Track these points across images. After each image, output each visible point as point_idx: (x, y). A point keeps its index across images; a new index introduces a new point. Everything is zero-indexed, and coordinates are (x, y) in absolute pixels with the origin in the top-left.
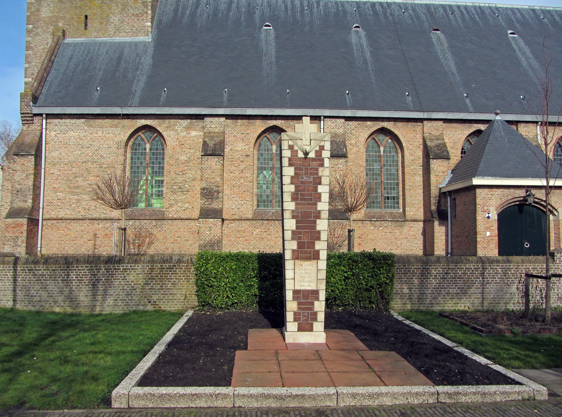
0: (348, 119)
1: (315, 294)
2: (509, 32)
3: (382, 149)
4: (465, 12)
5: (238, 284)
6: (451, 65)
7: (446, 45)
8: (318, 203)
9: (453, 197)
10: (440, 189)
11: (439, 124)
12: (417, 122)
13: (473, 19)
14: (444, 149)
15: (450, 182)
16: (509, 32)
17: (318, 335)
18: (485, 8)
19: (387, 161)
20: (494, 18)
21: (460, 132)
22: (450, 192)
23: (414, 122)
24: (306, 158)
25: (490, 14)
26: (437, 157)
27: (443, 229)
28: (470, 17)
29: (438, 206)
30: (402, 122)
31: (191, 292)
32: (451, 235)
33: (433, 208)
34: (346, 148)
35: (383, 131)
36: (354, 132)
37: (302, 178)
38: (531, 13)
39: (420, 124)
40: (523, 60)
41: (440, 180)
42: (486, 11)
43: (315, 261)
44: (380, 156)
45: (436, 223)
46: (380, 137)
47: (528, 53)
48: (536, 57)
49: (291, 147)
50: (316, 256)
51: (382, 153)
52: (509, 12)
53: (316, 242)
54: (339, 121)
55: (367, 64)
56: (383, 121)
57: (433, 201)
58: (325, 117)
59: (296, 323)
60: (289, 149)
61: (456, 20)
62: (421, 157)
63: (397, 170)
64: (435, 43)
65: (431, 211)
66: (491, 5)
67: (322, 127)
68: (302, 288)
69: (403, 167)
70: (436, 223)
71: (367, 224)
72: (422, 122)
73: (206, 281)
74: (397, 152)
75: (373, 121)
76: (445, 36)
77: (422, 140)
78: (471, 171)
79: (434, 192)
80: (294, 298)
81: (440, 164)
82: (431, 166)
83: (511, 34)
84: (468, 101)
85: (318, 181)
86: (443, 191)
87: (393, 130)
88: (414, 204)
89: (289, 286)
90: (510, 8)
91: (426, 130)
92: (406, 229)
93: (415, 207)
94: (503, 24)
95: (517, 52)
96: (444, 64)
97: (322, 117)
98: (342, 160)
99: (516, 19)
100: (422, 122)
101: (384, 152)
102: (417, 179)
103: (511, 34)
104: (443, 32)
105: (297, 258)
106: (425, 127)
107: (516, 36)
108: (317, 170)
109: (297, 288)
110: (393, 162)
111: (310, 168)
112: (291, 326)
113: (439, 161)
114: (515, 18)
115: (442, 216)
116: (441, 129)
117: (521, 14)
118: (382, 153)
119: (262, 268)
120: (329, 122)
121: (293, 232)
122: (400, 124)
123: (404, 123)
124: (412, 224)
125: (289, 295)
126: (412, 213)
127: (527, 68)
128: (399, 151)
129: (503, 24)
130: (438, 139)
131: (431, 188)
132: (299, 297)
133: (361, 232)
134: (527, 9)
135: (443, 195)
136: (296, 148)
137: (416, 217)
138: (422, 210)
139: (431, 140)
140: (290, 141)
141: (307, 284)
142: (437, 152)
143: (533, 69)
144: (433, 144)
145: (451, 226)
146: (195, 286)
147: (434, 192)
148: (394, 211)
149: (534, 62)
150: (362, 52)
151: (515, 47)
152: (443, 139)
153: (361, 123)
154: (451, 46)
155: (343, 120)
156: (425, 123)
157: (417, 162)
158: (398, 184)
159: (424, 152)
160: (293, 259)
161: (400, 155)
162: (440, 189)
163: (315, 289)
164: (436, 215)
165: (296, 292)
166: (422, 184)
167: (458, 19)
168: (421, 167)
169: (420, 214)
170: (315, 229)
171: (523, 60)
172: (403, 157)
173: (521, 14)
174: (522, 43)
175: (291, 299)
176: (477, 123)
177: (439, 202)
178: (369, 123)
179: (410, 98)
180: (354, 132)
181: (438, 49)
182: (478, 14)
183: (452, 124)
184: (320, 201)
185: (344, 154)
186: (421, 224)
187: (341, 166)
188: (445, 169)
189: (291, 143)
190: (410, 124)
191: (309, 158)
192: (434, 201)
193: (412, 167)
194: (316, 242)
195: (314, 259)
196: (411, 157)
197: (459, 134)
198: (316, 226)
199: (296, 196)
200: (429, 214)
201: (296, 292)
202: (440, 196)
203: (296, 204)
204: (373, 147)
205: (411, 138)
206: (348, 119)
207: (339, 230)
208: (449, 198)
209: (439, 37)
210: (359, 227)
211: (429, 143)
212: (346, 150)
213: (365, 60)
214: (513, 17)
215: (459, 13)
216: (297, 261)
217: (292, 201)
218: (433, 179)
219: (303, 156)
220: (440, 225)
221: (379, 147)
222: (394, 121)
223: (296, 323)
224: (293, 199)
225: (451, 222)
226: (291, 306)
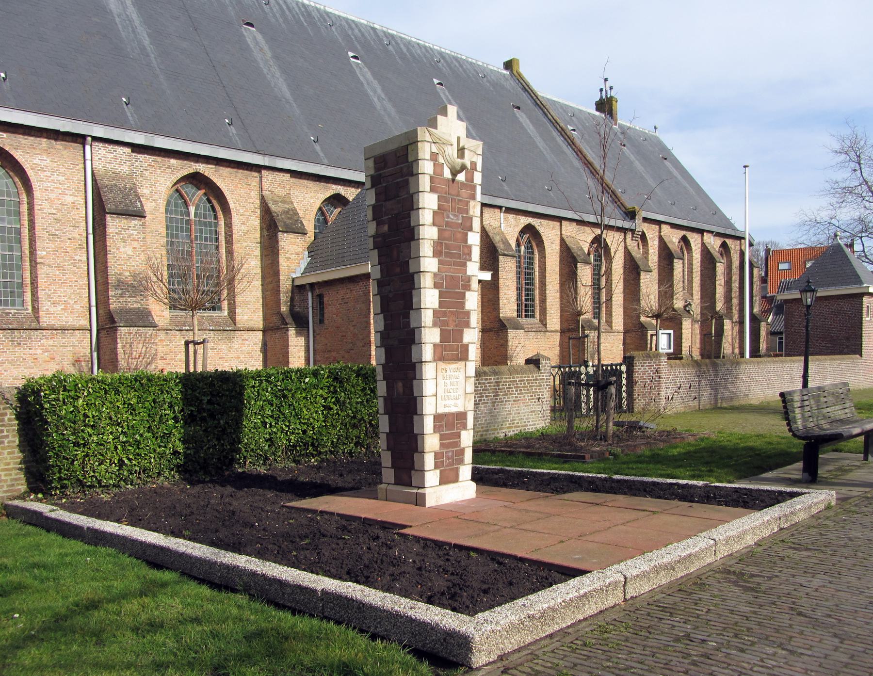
0: (137, 148)
1: (462, 416)
2: (351, 54)
3: (192, 209)
4: (285, 7)
5: (141, 436)
6: (283, 88)
7: (269, 54)
8: (468, 263)
9: (317, 292)
10: (293, 280)
11: (284, 178)
12: (251, 170)
13: (298, 21)
14: (295, 218)
15: (308, 269)
16: (351, 54)
17: (465, 489)
18: (311, 9)
19: (201, 231)
20: (326, 28)
21: (312, 194)
22: (312, 285)
23: (247, 170)
24: (453, 180)
25: (319, 20)
26: (289, 230)
27: (302, 340)
28: (294, 16)
29: (291, 305)
30: (229, 167)
31: (9, 464)
32: (314, 350)
33: (284, 309)
34: (140, 201)
35: (196, 179)
36: (147, 173)
37: (448, 217)
38: (372, 32)
39: (256, 174)
40: (376, 99)
41: (293, 266)
42: (313, 14)
43: (463, 363)
44: (188, 222)
45: (292, 332)
46: (188, 190)
47: (379, 91)
48: (390, 100)
49: (434, 157)
50: (462, 355)
51: (192, 216)
52: (344, 23)
53: (465, 330)
54: (121, 150)
55: (148, 56)
56: (197, 162)
57: (284, 298)
58: (95, 139)
59: (438, 471)
60: (431, 160)
61: (274, 16)
62: (258, 228)
63: (217, 248)
64: (252, 46)
65: (279, 314)
66: (318, 6)
67: (88, 156)
68: (447, 410)
69: (229, 241)
70: (292, 332)
71: (175, 336)
72: (260, 172)
73: (73, 434)
74: (216, 217)
75: (180, 159)
76: (264, 38)
77: (258, 202)
78: (328, 254)
79: (285, 285)
80: (436, 429)
81: (293, 240)
82: (280, 243)
83: (354, 57)
84: (317, 147)
85: (468, 224)
86: (297, 283)
87: (215, 180)
88: (248, 303)
89: (429, 407)
90: (344, 18)
91: (265, 185)
92: (237, 343)
93: (250, 306)
94: (340, 40)
95: (366, 85)
96: (273, 84)
97: (89, 139)
98: (135, 222)
99: (356, 37)
100: (260, 172)
101: (196, 214)
102: (253, 263)
103: (354, 57)
104: (261, 31)
105: (440, 360)
106: (264, 180)
107: (359, 62)
108: (467, 204)
109: (441, 410)
110: (211, 233)
111: (459, 201)
112: (432, 477)
113: (292, 235)
114: (353, 34)
115: (301, 323)
116: (287, 187)
117: (360, 31)
118: (192, 216)
119: (187, 400)
120: (101, 150)
121: (435, 312)
122: (225, 171)
123: (232, 170)
124: (246, 335)
125: (429, 424)
126: (246, 317)
127: (382, 113)
128: (220, 215)
129: (340, 40)
130: (284, 202)
131: (281, 277)
132: (442, 426)
133: (166, 349)
134: (366, 26)
135: (298, 289)
136: (441, 160)
137: (252, 324)
138: (261, 313)
139: (275, 202)
140: (433, 145)
141: (452, 402)
142: (288, 221)
143: (389, 115)
144: (280, 209)
145: (314, 337)
146: (17, 450)
147: (285, 285)
148: (215, 314)
149: (389, 106)
150: (133, 31)
151: (362, 78)
152: (292, 203)
153: (159, 159)
154: (276, 57)
155: (128, 150)
156: (264, 173)
157: (252, 236)
158: (21, 285)
159: (262, 219)
160: (435, 360)
161: (222, 223)
162: (293, 280)
163: (462, 410)
164: (289, 320)
165: (438, 418)
166: (259, 271)
167: (278, 15)
168: (259, 245)
169: (258, 320)
170: (463, 308)
171: (376, 99)
172: (229, 225)
173: (360, 31)
174: (369, 75)
175: (432, 431)
176: (335, 184)
177: (292, 299)
178: (173, 161)
179: (233, 130)
180: (147, 173)
181: (258, 56)
182: (303, 15)
183: (302, 181)
184: (470, 260)
185: (139, 211)
186: (260, 335)
187: (135, 233)
188: (300, 250)
189: (435, 149)
190: (241, 173)
191: (458, 182)
192: (285, 299)
193: (245, 244)
194: (465, 330)
195: (461, 360)
196: (243, 228)
197: (311, 197)
198: (464, 303)
199: (439, 248)
200: (275, 320)
201: (438, 418)
202: (292, 292)
203: (440, 262)
204: (176, 205)
205: (242, 194)
206: (137, 148)
207: (141, 345)
208: (310, 294)
209: (255, 37)
210: (162, 341)
211: (273, 207)
212: (142, 205)
213: (143, 49)
214: (350, 32)
215: (277, 7)
216: (440, 364)
217: (434, 256)
218: (283, 263)
219: (450, 177)
220: (298, 334)
221: (186, 205)
222: (216, 165)
223: (438, 471)
224: (437, 253)
225: (314, 331)
226: (431, 442)
